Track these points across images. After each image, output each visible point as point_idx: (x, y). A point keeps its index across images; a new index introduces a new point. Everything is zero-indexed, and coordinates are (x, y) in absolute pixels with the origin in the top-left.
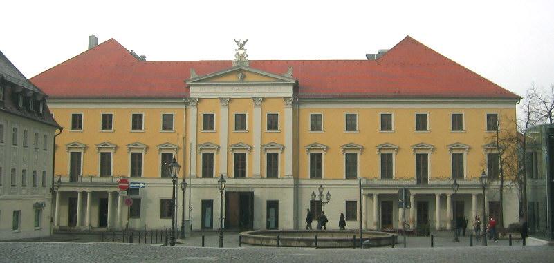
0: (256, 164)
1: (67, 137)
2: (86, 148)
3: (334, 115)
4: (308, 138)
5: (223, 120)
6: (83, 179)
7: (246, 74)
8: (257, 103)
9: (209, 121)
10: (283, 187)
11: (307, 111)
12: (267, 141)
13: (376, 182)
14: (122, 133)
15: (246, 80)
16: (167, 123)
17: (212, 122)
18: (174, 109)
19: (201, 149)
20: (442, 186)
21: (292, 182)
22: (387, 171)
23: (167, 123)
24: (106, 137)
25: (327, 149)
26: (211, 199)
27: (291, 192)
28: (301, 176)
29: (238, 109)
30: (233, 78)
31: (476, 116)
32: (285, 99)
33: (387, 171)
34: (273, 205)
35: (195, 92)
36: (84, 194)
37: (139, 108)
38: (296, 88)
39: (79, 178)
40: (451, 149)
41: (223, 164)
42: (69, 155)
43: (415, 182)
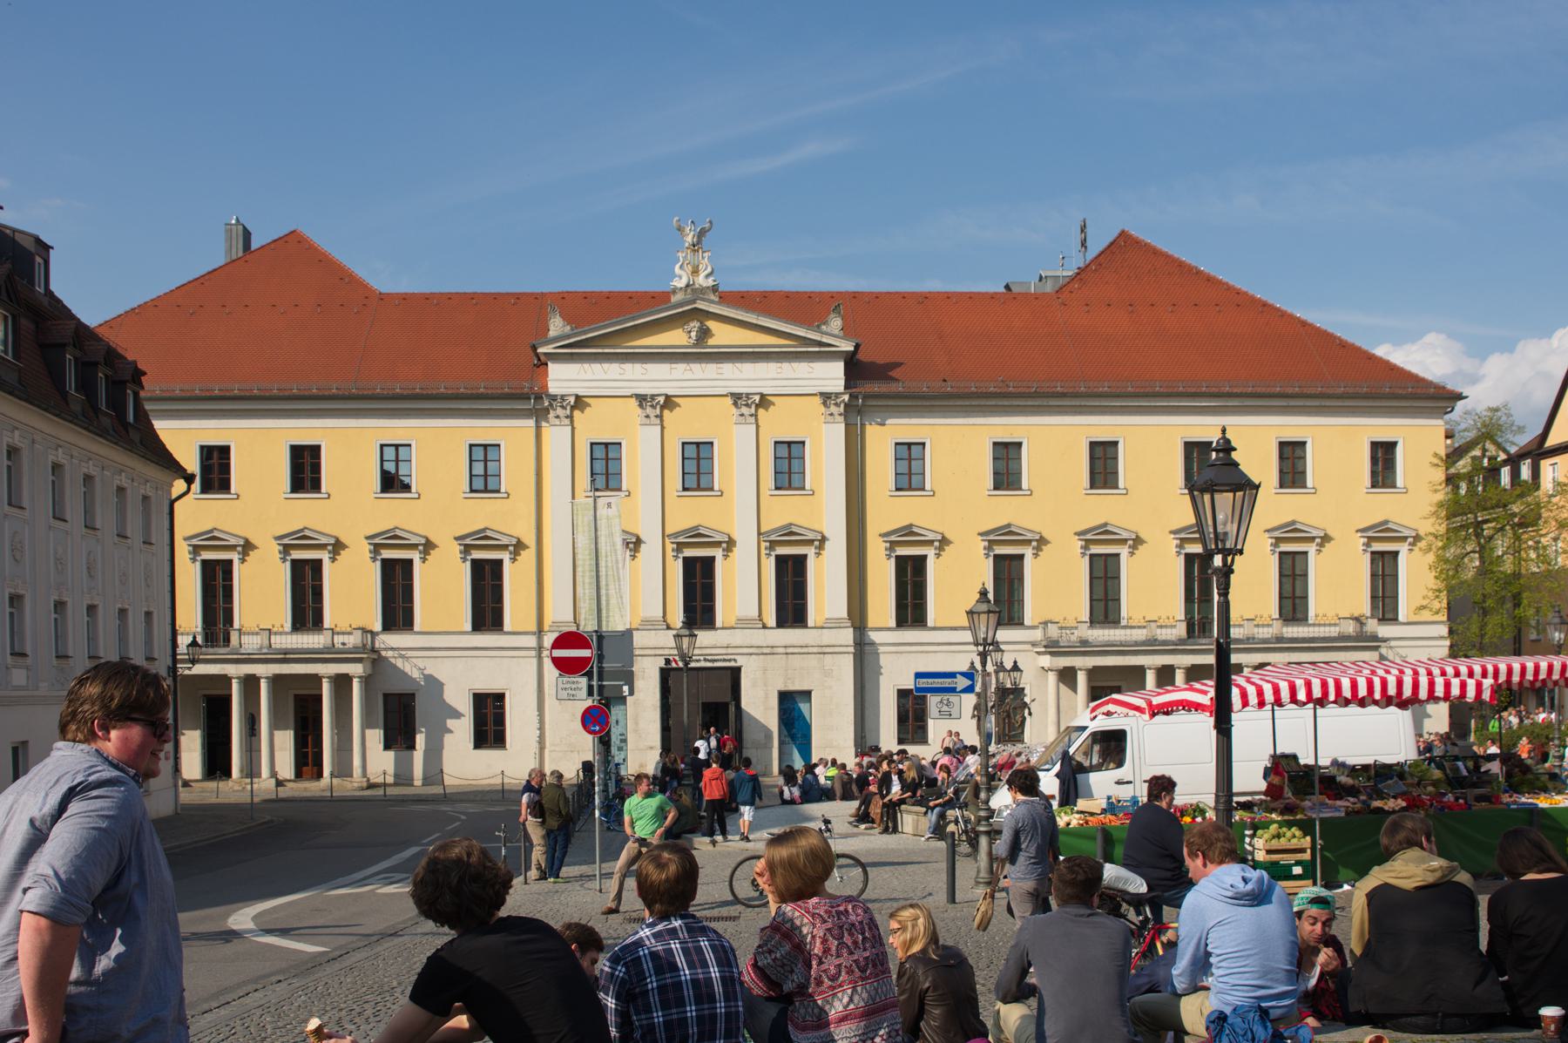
0: (743, 586)
1: (195, 513)
2: (338, 547)
3: (958, 444)
4: (887, 510)
5: (646, 457)
6: (245, 639)
7: (711, 324)
8: (745, 410)
9: (605, 466)
10: (823, 651)
11: (882, 438)
12: (772, 522)
13: (280, 642)
14: (350, 508)
15: (711, 342)
16: (484, 473)
17: (225, 468)
18: (510, 434)
19: (773, 545)
20: (1165, 643)
21: (847, 636)
22: (1105, 606)
23: (484, 473)
24: (306, 512)
25: (1138, 541)
26: (776, 695)
27: (847, 665)
28: (872, 621)
29: (685, 425)
30: (676, 338)
31: (1420, 442)
32: (826, 397)
33: (1105, 606)
34: (791, 705)
35: (562, 378)
36: (250, 683)
37: (305, 430)
38: (855, 369)
39: (234, 637)
40: (1278, 540)
41: (957, 582)
42: (377, 568)
43: (1181, 631)
